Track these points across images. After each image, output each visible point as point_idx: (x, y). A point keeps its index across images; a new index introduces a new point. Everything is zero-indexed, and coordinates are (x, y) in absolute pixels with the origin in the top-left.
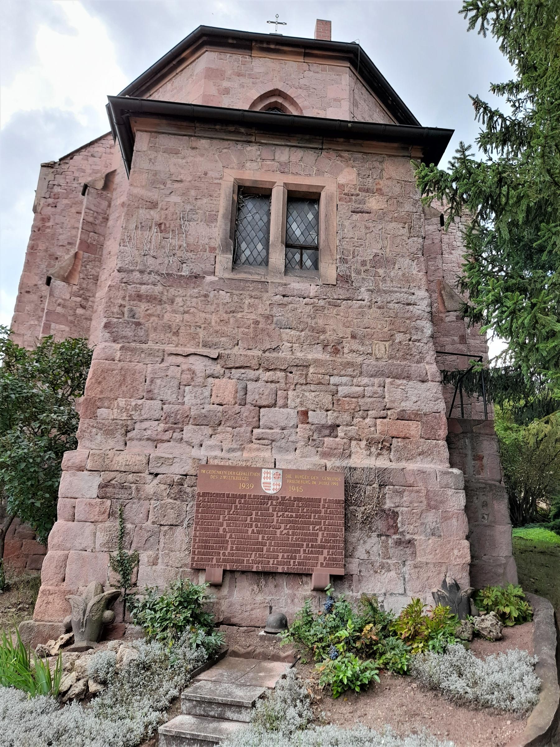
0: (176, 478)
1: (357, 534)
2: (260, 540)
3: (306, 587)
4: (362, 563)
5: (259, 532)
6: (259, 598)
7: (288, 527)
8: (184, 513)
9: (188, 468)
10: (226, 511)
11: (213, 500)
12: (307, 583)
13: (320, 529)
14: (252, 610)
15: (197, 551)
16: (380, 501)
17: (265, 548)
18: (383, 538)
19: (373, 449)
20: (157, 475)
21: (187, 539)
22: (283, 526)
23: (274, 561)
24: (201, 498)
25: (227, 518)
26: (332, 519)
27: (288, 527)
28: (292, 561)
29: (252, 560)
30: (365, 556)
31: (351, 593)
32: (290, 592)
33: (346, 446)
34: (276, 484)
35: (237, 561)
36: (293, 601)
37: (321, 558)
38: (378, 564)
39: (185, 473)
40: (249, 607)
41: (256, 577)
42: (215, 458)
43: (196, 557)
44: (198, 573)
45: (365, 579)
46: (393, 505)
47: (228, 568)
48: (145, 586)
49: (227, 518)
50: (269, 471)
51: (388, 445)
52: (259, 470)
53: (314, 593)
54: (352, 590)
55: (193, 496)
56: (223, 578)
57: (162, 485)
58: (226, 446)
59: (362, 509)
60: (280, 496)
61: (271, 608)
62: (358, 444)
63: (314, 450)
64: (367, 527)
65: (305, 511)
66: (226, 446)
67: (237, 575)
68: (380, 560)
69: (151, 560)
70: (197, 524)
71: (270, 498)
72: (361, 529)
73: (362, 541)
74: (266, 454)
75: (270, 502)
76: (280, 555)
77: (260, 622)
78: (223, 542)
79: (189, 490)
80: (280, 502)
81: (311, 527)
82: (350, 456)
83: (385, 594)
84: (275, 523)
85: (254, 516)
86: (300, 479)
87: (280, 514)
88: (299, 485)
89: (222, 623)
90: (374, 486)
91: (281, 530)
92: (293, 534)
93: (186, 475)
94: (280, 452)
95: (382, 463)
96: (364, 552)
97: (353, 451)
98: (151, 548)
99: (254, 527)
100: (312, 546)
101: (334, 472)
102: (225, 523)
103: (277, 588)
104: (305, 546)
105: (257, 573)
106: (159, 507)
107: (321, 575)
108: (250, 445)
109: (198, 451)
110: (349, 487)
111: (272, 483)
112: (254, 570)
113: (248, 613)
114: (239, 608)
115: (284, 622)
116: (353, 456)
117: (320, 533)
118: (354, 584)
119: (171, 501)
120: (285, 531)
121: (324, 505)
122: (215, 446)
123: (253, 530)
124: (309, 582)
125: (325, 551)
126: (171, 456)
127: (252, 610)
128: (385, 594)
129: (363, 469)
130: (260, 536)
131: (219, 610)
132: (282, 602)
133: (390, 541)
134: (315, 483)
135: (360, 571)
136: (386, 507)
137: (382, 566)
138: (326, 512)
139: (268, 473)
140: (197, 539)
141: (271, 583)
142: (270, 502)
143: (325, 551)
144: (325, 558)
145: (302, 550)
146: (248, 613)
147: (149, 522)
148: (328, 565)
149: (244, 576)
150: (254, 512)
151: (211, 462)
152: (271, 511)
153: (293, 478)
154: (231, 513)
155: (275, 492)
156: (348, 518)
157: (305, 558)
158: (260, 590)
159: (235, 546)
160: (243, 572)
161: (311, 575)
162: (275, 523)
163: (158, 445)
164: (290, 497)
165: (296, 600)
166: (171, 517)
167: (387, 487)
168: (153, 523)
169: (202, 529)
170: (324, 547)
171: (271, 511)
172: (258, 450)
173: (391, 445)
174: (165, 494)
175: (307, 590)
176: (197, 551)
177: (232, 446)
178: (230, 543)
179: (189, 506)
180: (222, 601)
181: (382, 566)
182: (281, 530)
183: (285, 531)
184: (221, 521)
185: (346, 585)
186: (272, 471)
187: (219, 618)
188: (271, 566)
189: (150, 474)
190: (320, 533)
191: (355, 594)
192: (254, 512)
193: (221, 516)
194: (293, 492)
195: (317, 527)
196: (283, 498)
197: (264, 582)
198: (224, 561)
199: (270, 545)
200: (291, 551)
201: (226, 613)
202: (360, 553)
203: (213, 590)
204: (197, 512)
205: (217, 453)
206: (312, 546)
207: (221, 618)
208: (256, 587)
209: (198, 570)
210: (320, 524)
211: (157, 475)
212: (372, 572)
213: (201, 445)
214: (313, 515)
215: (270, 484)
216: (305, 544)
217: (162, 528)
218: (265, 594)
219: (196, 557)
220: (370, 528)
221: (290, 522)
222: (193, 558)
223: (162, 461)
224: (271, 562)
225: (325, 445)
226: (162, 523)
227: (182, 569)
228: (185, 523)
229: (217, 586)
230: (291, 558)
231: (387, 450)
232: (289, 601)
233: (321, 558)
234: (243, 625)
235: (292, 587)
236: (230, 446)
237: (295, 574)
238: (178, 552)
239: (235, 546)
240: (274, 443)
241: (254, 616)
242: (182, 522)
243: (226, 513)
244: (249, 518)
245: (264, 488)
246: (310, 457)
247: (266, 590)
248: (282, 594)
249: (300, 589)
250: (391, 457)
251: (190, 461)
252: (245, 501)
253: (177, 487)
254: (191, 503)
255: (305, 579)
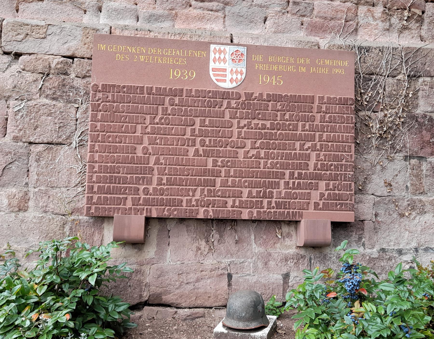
0: (55, 61)
1: (372, 156)
2: (210, 166)
3: (288, 242)
4: (379, 202)
5: (207, 154)
6: (209, 262)
7: (257, 145)
8: (73, 123)
9: (74, 45)
10: (148, 117)
11: (123, 98)
12: (289, 235)
13: (313, 148)
14: (198, 280)
15: (96, 187)
16: (410, 103)
17: (219, 180)
18: (413, 161)
19: (395, 20)
20: (18, 55)
21: (78, 167)
22: (249, 143)
23: (234, 202)
24: (100, 95)
25: (149, 130)
26: (333, 130)
27: (257, 145)
28: (265, 201)
29: (197, 200)
30: (385, 191)
31: (361, 249)
32: (262, 249)
33: (350, 14)
34: (237, 72)
35: (169, 203)
36: (266, 264)
37: (315, 196)
38: (406, 203)
39: (69, 54)
40: (192, 277)
41: (204, 227)
42: (125, 28)
43: (96, 197)
44: (103, 222)
45: (384, 227)
46: (430, 109)
47: (154, 215)
48: (5, 246)
49: (149, 130)
50: (222, 47)
51: (419, 12)
52: (205, 46)
53: (302, 252)
54: (364, 245)
55: (87, 93)
56: (145, 235)
57: (29, 74)
58: (144, 10)
59: (380, 115)
60: (242, 93)
61: (230, 276)
62: (369, 10)
63: (296, 20)
64: (387, 145)
65: (287, 117)
66: (144, 10)
67: (171, 226)
68: (409, 196)
69: (15, 202)
70: (95, 139)
71: (226, 95)
72: (378, 148)
73: (378, 167)
74: (216, 26)
75: (225, 102)
76: (246, 191)
77: (212, 300)
78: (144, 171)
79: (78, 83)
80: (244, 103)
81: (298, 144)
82: (356, 30)
83: (416, 250)
84: (234, 139)
85: (197, 126)
86: (278, 64)
87: (245, 122)
88: (277, 73)
89: (146, 303)
90: (399, 77)
91: (246, 149)
92: (267, 157)
93: (72, 58)
94: (239, 23)
95: (409, 41)
96: (382, 184)
97: (361, 22)
98: (13, 182)
99: (198, 146)
100: (300, 176)
101: (334, 52)
102: (146, 138)
103: (237, 245)
104: (287, 176)
105: (206, 221)
106: (24, 112)
107: (315, 223)
108: (186, 11)
109: (95, 19)
110: (363, 79)
111: (229, 70)
112: (201, 216)
113: (190, 287)
114: (176, 278)
115: (260, 308)
116: (361, 31)
117: (314, 155)
118: (367, 234)
119: (47, 101)
120: (254, 152)
121: (319, 108)
122: (125, 10)
123: (197, 151)
124: (293, 233)
125: (322, 184)
126: (43, 23)
127: (198, 280)
128: (416, 250)
129: (381, 50)
130: (210, 160)
131: (140, 282)
132: (249, 263)
133: (425, 166)
134: (304, 70)
135: (376, 215)
136: (419, 111)
137: (412, 206)
138: (323, 120)
139: (220, 52)
140: (97, 165)
141: (230, 238)
142: (225, 102)
143: (322, 184)
144: (322, 195)
145: (282, 182)
146: (190, 287)
147: (8, 139)
148: (326, 207)
149: (183, 227)
150: (198, 120)
151: (117, 32)
152: (227, 117)
153: (265, 61)
154: (157, 120)
155: (234, 85)
156: (361, 128)
157: (288, 196)
158: (210, 249)
159: (165, 178)
160: (182, 220)
161: (297, 223)
162: (234, 139)
163: (21, 7)
164: (261, 95)
165: (272, 263)
166: (48, 130)
167: (421, 80)
168: (16, 139)
169: (104, 149)
170: (319, 178)
171: (227, 117)
172: (201, 18)
173: (423, 12)
174: (34, 89)
175: (289, 247)
176: (96, 187)
177: (155, 12)
178: (156, 172)
179: (80, 111)
180: (146, 269)
181: (412, 206)
182: (246, 149)
183: (254, 152)
184: (138, 134)
185: (354, 236)
186: (227, 48)
187: (141, 296)
188: (229, 209)
189: (5, 53)
190: (314, 155)
191: (368, 251)
192: (198, 120)
193: (139, 127)
194: (267, 84)
195: (308, 145)
196: (249, 96)
197: (217, 236)
198: (147, 202)
199: (228, 175)
200: (264, 185)
201: (153, 288)
202: (377, 185)
203: (130, 251)
204: (94, 118)
205: (130, 22)
206: (300, 176)
207: (146, 296)
208: (203, 243)
209: (101, 219)
210: (312, 138)
211: (18, 55)
212: (395, 215)
213: (100, 9)
214: (300, 124)
215: (226, 71)
216: (287, 172)
217: (32, 147)
218: (220, 254)
219: (96, 197)
220: (393, 147)
221: (261, 136)
222: (90, 199)
223: (28, 31)
224: (230, 202)
225: (315, 12)
226: (32, 139)
227: (73, 217)
228: (75, 140)
229: (137, 245)
230: (264, 197)
231: (417, 21)
232: (260, 265)
233: (315, 196)
234: (184, 305)
235: (265, 243)
236: (150, 11)
237: (269, 221)
238: (64, 190)
239: (165, 178)
240: (228, 8)
241: (201, 291)
242: (69, 137)
243: (148, 121)
244: (189, 129)
245: (214, 78)
246: (290, 31)
247: (222, 247)
248: (249, 253)
249: (278, 245)
250: (423, 33)
251: (79, 33)
252: (181, 101)
253: (59, 75)
254: (84, 106)
255: (285, 229)
